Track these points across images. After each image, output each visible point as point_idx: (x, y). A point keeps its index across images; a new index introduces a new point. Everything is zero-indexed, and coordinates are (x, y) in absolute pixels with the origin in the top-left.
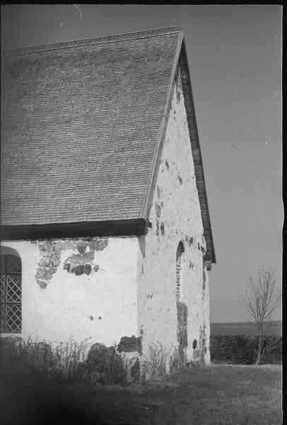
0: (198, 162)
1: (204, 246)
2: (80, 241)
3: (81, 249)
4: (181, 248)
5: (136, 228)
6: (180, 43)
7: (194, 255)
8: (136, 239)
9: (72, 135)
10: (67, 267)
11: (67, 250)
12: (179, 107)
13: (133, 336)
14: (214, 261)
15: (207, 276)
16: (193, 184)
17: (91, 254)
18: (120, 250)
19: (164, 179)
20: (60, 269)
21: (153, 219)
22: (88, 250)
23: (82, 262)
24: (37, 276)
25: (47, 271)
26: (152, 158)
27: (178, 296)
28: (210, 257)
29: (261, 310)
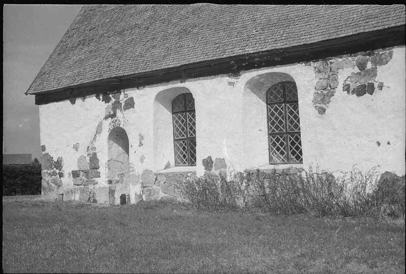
2: (360, 57)
3: (362, 66)
10: (347, 88)
13: (73, 102)
22: (369, 65)
23: (363, 81)
24: (315, 101)
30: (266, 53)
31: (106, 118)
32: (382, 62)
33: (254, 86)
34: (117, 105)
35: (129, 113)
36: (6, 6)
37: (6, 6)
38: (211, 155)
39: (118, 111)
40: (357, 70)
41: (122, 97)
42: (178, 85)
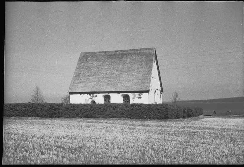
0: (159, 72)
1: (161, 89)
2: (139, 93)
3: (139, 95)
4: (155, 91)
5: (148, 92)
6: (154, 52)
7: (158, 92)
8: (147, 93)
9: (136, 73)
10: (137, 97)
11: (137, 95)
12: (155, 64)
13: (81, 95)
14: (163, 92)
15: (161, 95)
16: (158, 78)
17: (141, 96)
18: (145, 94)
19: (152, 81)
20: (136, 98)
21: (150, 89)
22: (140, 95)
23: (139, 97)
24: (132, 99)
25: (134, 98)
26: (151, 67)
27: (155, 100)
28: (162, 91)
29: (18, 148)
30: (189, 103)
31: (90, 98)
32: (141, 94)
33: (122, 95)
34: (93, 96)
35: (96, 98)
36: (5, 162)
37: (5, 162)
38: (98, 98)
39: (93, 98)
40: (138, 95)
41: (94, 95)
42: (107, 94)
